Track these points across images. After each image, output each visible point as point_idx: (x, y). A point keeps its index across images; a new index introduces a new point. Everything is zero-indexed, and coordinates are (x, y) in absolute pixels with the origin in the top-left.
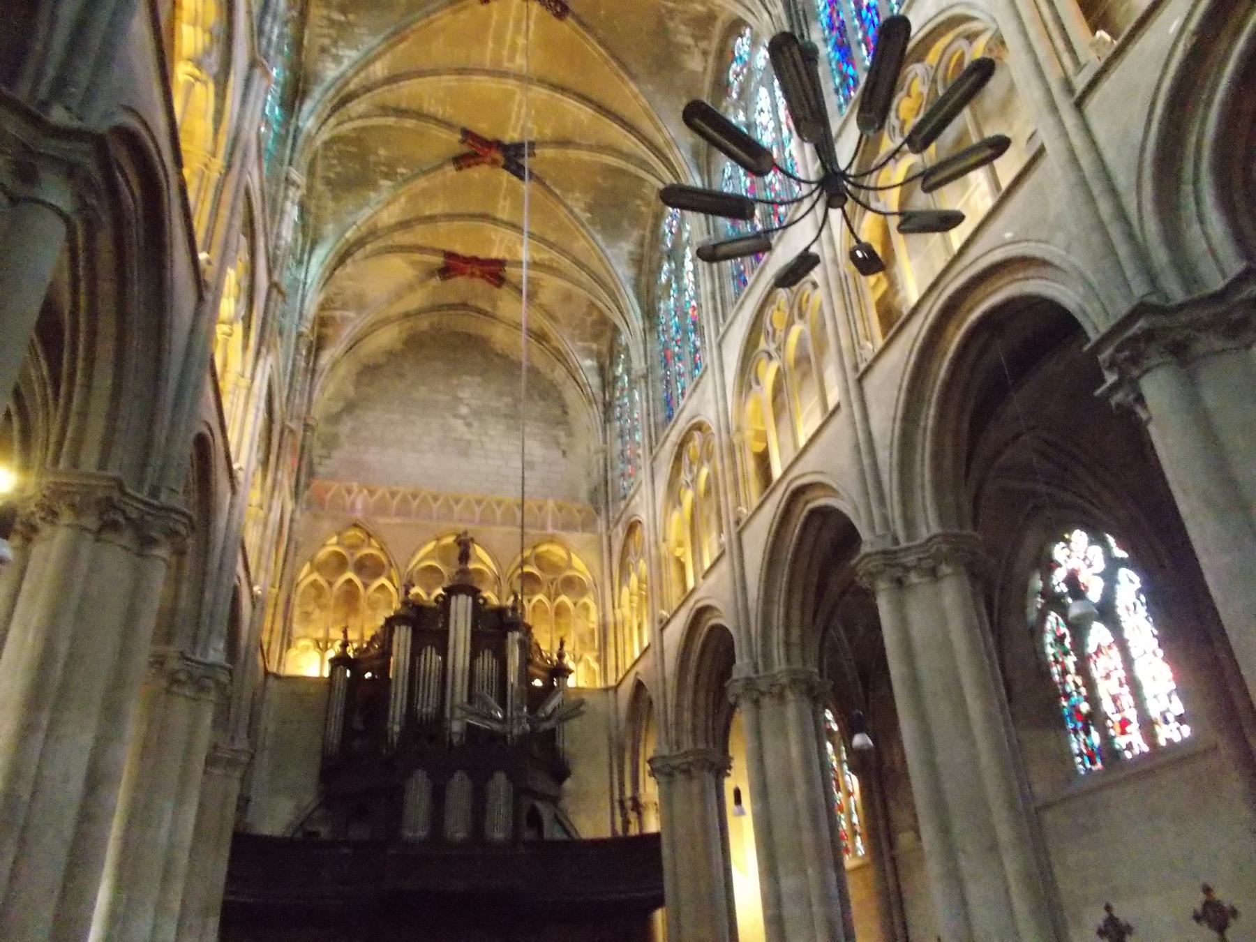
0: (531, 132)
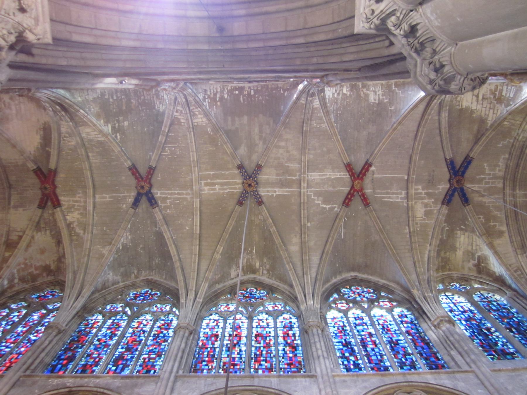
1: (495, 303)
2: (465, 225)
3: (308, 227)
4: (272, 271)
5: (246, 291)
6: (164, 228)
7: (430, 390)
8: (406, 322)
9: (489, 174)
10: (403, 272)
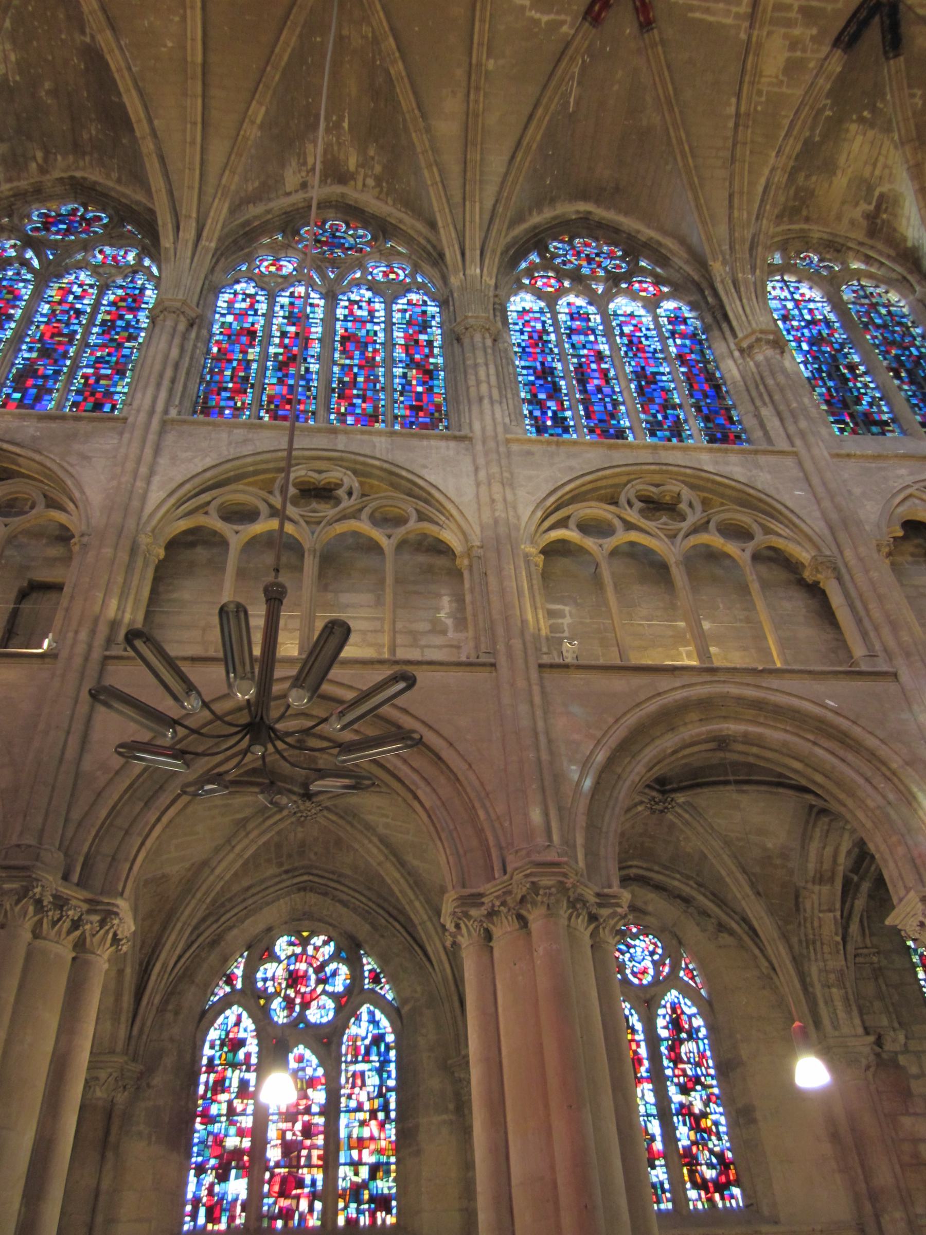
1: (883, 311)
2: (874, 109)
3: (486, 71)
4: (388, 181)
5: (322, 226)
6: (105, 39)
7: (701, 483)
8: (683, 336)
10: (701, 215)
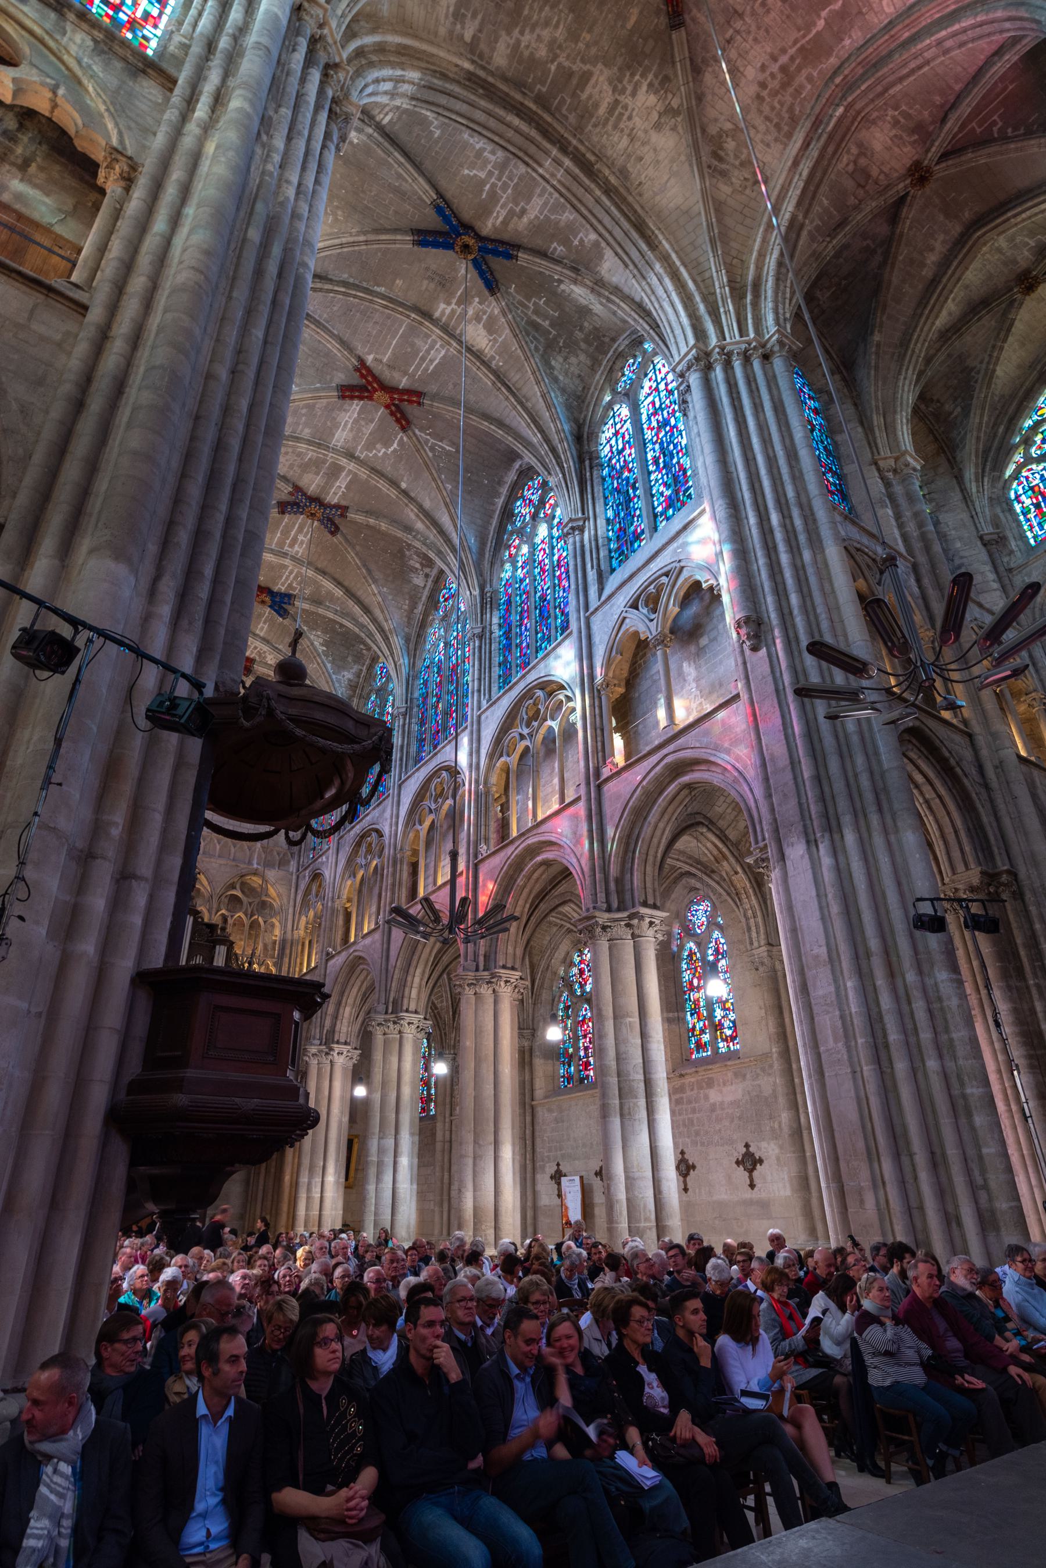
0: (295, 589)
9: (490, 174)
